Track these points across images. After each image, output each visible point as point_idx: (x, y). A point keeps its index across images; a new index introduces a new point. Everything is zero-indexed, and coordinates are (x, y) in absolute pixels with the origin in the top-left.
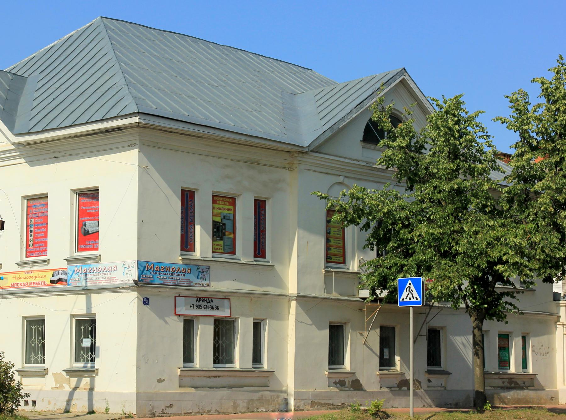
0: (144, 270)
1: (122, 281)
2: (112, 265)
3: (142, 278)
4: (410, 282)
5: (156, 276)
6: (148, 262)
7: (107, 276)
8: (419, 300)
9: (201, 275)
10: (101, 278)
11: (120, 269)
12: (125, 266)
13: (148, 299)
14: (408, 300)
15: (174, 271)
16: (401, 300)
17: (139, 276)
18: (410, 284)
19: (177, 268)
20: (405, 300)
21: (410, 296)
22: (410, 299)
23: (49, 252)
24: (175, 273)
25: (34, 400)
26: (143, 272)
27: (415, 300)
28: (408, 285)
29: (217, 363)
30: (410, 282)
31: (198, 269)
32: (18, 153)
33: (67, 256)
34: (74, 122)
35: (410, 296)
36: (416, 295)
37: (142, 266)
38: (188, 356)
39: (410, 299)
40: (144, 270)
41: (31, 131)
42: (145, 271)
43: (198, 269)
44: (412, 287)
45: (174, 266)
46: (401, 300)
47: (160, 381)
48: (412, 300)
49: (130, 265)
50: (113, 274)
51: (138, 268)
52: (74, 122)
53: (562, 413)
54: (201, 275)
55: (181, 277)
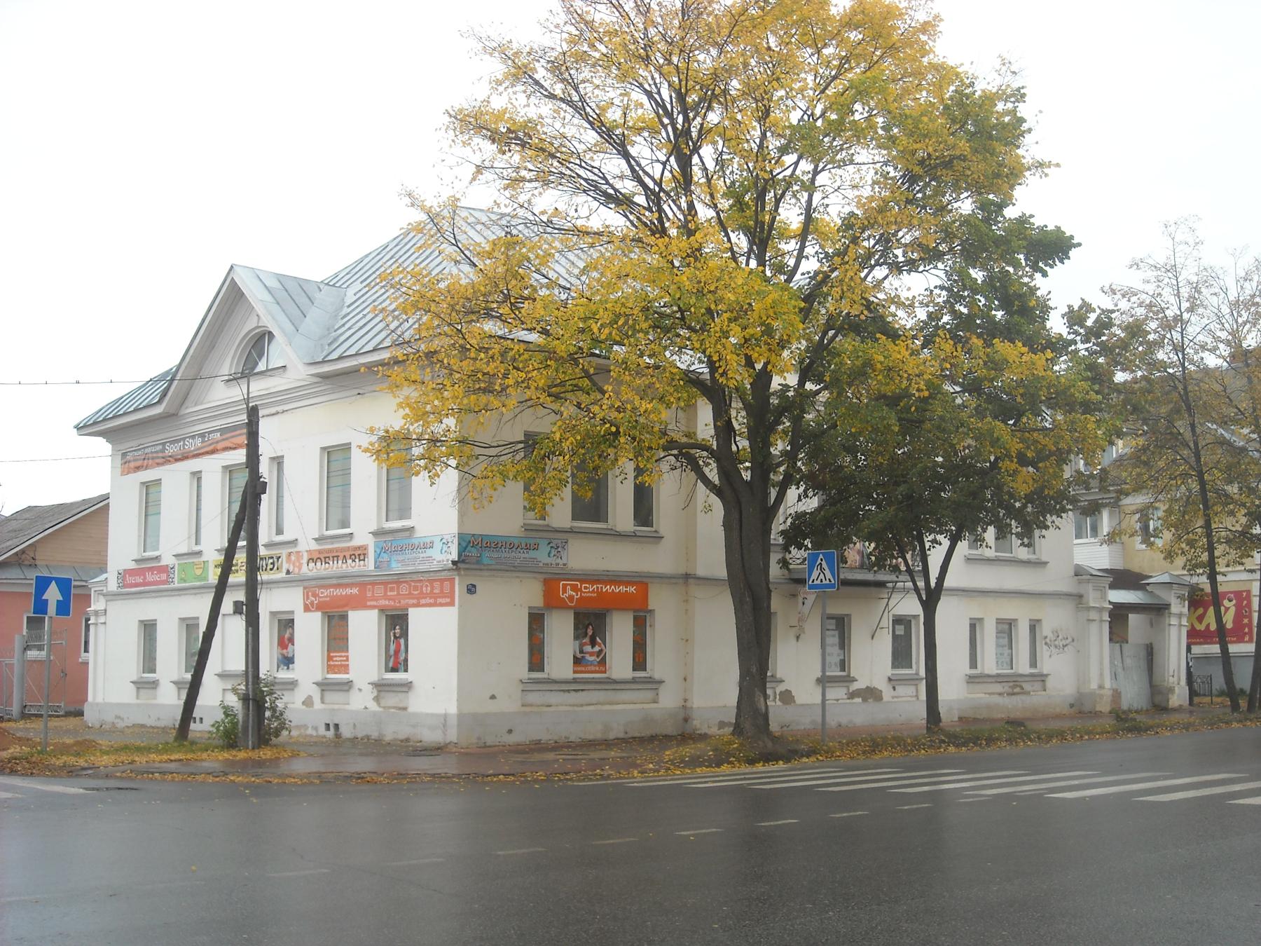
0: (467, 546)
1: (440, 562)
2: (428, 540)
3: (463, 557)
4: (821, 556)
5: (486, 554)
6: (473, 535)
7: (422, 555)
8: (833, 582)
9: (553, 552)
10: (415, 558)
11: (438, 545)
12: (444, 541)
13: (474, 586)
14: (819, 582)
15: (512, 547)
16: (810, 583)
17: (460, 555)
18: (822, 560)
19: (516, 542)
20: (815, 582)
21: (822, 576)
22: (821, 581)
23: (161, 546)
24: (514, 549)
25: (337, 722)
26: (465, 548)
27: (828, 582)
28: (819, 561)
29: (576, 669)
30: (821, 556)
31: (549, 543)
32: (330, 386)
33: (374, 528)
34: (345, 351)
35: (822, 576)
36: (829, 575)
37: (464, 540)
38: (536, 660)
39: (821, 581)
40: (467, 546)
41: (326, 359)
42: (469, 548)
43: (549, 543)
44: (824, 563)
45: (512, 539)
46: (810, 583)
47: (493, 697)
48: (824, 582)
49: (450, 540)
50: (429, 552)
51: (459, 544)
52: (345, 351)
53: (983, 719)
54: (553, 552)
55: (523, 555)
